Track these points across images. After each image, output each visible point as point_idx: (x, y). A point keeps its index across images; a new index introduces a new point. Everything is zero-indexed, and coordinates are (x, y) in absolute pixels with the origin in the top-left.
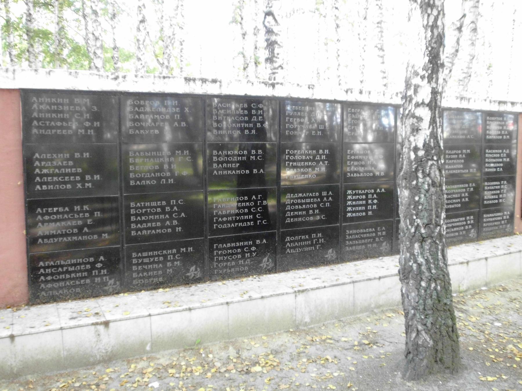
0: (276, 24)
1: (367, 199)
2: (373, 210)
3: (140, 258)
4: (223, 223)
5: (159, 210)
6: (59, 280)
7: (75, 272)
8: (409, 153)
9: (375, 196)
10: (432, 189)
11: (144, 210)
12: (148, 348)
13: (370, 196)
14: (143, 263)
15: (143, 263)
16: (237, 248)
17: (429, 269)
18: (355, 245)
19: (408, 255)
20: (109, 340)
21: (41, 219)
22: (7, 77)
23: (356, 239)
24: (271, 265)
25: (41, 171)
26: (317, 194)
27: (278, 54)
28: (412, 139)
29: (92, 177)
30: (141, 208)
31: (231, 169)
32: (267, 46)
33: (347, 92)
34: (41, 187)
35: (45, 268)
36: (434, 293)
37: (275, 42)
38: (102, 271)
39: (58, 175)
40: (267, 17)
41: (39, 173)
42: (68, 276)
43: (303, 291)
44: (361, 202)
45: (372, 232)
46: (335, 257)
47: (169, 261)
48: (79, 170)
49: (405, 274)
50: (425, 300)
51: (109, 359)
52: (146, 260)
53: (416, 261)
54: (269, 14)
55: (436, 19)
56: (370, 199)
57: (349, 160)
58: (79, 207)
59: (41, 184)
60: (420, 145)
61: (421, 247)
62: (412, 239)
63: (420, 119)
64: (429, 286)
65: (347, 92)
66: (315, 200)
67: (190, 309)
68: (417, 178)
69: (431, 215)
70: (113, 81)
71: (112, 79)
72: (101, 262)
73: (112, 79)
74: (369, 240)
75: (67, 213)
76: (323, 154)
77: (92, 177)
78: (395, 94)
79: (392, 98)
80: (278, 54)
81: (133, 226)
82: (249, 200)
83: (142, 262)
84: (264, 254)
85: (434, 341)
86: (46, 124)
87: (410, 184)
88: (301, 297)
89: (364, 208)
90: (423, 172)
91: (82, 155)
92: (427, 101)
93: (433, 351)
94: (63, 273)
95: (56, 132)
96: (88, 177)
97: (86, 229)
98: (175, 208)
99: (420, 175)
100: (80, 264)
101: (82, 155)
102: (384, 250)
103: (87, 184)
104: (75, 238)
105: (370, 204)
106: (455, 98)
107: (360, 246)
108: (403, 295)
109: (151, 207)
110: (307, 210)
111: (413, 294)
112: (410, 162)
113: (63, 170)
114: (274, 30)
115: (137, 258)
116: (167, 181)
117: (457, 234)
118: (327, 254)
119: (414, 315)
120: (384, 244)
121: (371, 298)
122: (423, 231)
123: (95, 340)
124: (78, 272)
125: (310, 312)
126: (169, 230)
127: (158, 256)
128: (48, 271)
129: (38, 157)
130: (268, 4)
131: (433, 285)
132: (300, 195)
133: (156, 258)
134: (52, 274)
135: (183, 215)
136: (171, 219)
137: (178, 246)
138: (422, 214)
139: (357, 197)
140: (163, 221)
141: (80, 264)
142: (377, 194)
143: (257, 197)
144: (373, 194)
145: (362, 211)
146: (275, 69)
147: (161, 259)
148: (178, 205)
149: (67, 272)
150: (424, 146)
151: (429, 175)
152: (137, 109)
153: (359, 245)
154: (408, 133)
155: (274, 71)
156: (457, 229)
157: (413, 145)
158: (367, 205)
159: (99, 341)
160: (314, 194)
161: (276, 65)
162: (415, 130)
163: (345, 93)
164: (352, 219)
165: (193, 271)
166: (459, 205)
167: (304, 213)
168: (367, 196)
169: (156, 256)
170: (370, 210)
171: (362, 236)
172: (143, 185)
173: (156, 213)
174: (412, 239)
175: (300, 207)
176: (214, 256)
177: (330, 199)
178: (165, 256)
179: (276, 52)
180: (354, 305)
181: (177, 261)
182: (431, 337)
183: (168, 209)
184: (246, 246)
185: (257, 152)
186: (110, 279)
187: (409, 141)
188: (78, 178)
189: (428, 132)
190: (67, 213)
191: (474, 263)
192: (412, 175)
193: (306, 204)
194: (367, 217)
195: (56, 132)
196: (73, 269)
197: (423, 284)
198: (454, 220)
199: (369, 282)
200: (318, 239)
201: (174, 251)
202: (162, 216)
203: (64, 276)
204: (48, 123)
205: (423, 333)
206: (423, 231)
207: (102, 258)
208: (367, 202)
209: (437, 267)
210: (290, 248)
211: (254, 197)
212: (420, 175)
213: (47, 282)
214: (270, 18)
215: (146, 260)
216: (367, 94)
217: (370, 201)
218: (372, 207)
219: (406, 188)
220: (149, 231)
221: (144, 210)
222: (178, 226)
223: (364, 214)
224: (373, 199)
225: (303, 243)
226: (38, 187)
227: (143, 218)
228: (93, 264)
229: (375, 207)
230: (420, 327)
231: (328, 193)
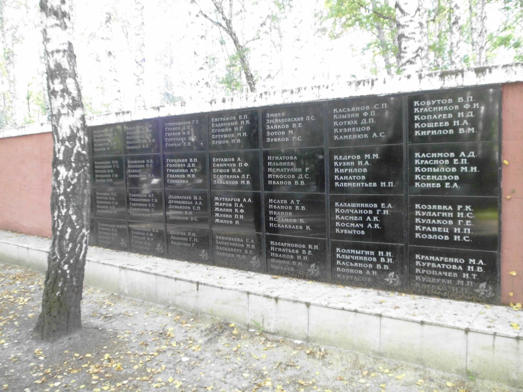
0: (403, 15)
1: (233, 208)
9: (241, 205)
13: (236, 205)
18: (225, 251)
23: (225, 246)
24: (398, 283)
26: (190, 198)
27: (405, 48)
33: (211, 103)
44: (227, 210)
56: (236, 208)
57: (215, 168)
65: (211, 103)
74: (238, 250)
76: (193, 162)
78: (259, 95)
79: (255, 101)
84: (482, 281)
88: (123, 271)
89: (231, 216)
102: (254, 264)
105: (237, 213)
106: (347, 84)
107: (230, 254)
117: (361, 272)
118: (200, 253)
120: (254, 258)
121: (169, 295)
125: (128, 286)
132: (178, 197)
139: (224, 204)
142: (244, 204)
143: (295, 202)
153: (229, 252)
156: (361, 265)
158: (233, 213)
160: (282, 201)
163: (210, 104)
166: (363, 232)
168: (233, 204)
170: (237, 219)
171: (353, 257)
172: (342, 187)
175: (178, 207)
177: (200, 203)
191: (286, 303)
193: (182, 205)
198: (353, 251)
199: (167, 279)
200: (193, 237)
208: (234, 210)
211: (292, 201)
216: (230, 101)
217: (236, 210)
218: (239, 217)
223: (447, 238)
224: (239, 209)
231: (198, 198)
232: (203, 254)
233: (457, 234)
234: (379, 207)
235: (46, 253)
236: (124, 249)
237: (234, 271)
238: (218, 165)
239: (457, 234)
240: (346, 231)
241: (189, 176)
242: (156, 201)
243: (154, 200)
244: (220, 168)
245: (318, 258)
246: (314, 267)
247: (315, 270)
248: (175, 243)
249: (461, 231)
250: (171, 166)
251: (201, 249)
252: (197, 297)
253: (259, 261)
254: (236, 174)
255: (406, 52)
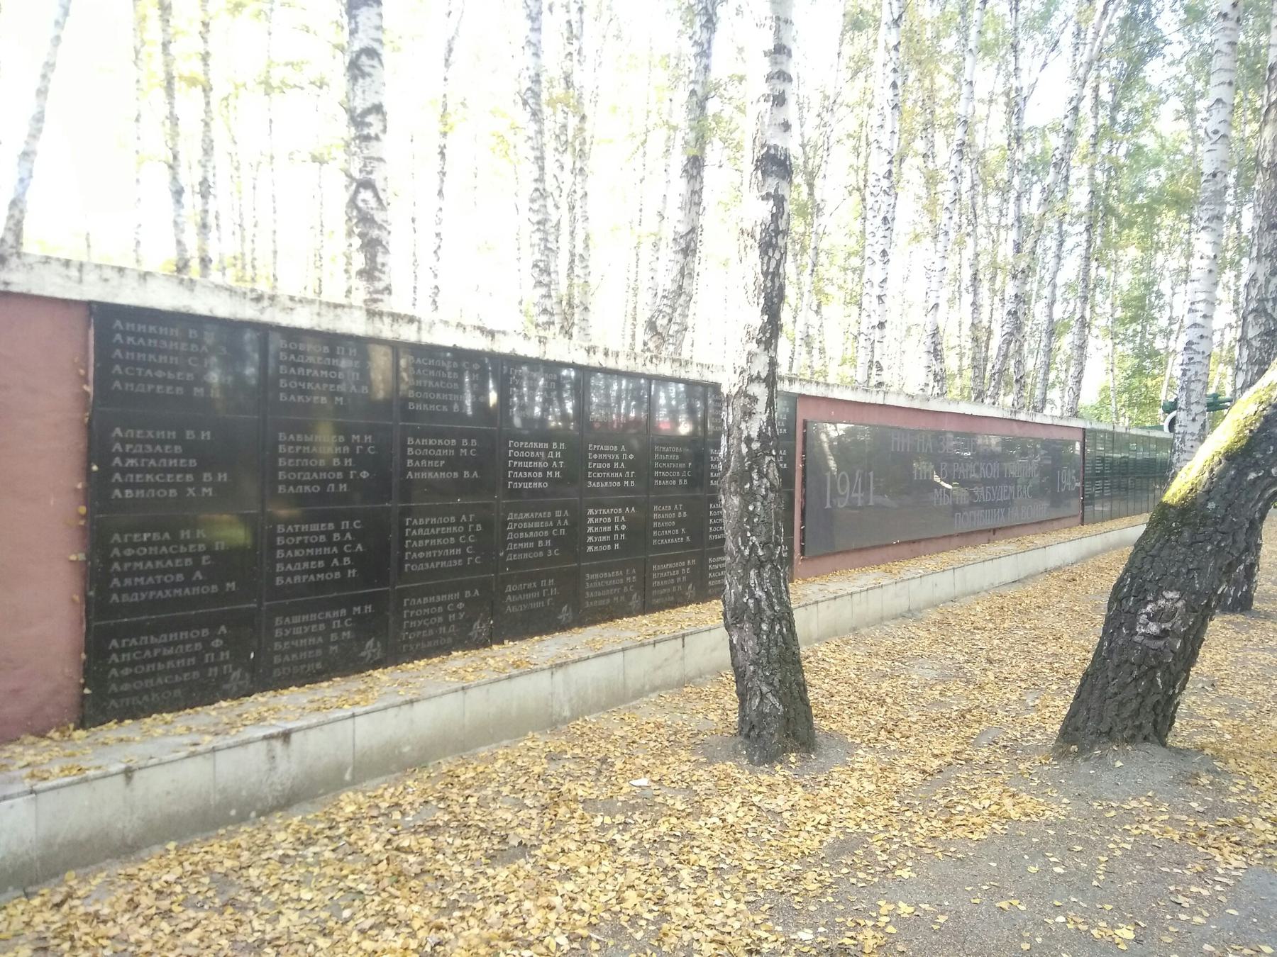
2: (620, 541)
3: (288, 626)
4: (418, 561)
5: (322, 538)
6: (144, 676)
7: (173, 657)
8: (739, 445)
10: (771, 495)
11: (299, 539)
12: (348, 777)
14: (292, 637)
15: (292, 637)
16: (437, 605)
17: (771, 606)
19: (740, 587)
20: (290, 765)
21: (118, 554)
22: (68, 277)
25: (124, 462)
26: (453, 519)
27: (383, 265)
28: (743, 426)
29: (215, 476)
30: (294, 535)
31: (434, 469)
32: (362, 247)
33: (588, 352)
34: (123, 494)
35: (119, 652)
36: (780, 639)
37: (378, 242)
38: (222, 654)
39: (154, 471)
40: (362, 190)
41: (121, 465)
42: (160, 666)
43: (561, 665)
45: (619, 577)
46: (571, 618)
47: (334, 631)
48: (193, 463)
49: (734, 618)
50: (768, 650)
51: (288, 800)
52: (297, 631)
53: (752, 596)
54: (367, 184)
55: (778, 265)
58: (188, 532)
59: (123, 487)
60: (754, 434)
61: (759, 575)
62: (747, 564)
63: (754, 399)
64: (772, 628)
66: (547, 525)
67: (411, 702)
68: (751, 479)
69: (770, 530)
70: (253, 304)
71: (252, 299)
72: (222, 636)
73: (252, 299)
75: (167, 544)
76: (558, 450)
77: (215, 476)
80: (383, 265)
81: (279, 567)
82: (458, 523)
83: (291, 634)
85: (784, 707)
86: (136, 372)
87: (742, 488)
88: (559, 675)
90: (760, 472)
91: (198, 434)
92: (763, 375)
93: (784, 721)
94: (150, 661)
95: (154, 390)
96: (207, 476)
97: (198, 575)
98: (348, 536)
99: (755, 476)
100: (184, 642)
101: (198, 434)
103: (204, 490)
104: (178, 592)
108: (732, 647)
109: (310, 533)
110: (535, 540)
111: (751, 643)
112: (741, 458)
113: (164, 460)
114: (376, 218)
115: (283, 627)
116: (337, 487)
119: (754, 672)
122: (760, 553)
123: (268, 766)
124: (180, 658)
125: (570, 700)
126: (338, 575)
127: (318, 622)
128: (126, 657)
129: (120, 434)
130: (365, 166)
131: (777, 628)
133: (314, 626)
134: (132, 664)
135: (359, 547)
136: (466, 533)
137: (349, 603)
138: (758, 529)
140: (328, 558)
141: (184, 642)
144: (620, 515)
145: (606, 543)
146: (377, 292)
147: (322, 627)
148: (353, 532)
149: (163, 659)
150: (759, 436)
151: (766, 476)
152: (292, 357)
154: (738, 418)
155: (375, 296)
157: (745, 434)
159: (273, 769)
161: (380, 285)
162: (748, 414)
164: (594, 555)
165: (371, 647)
167: (532, 545)
169: (313, 622)
173: (318, 545)
174: (747, 564)
176: (403, 620)
178: (328, 622)
179: (380, 259)
180: (625, 686)
181: (346, 629)
182: (781, 702)
183: (336, 536)
184: (451, 601)
185: (469, 442)
186: (235, 669)
187: (739, 428)
188: (189, 478)
189: (764, 418)
190: (167, 544)
192: (744, 476)
193: (533, 530)
194: (613, 553)
195: (154, 390)
196: (170, 652)
197: (764, 627)
200: (549, 588)
201: (343, 612)
202: (327, 550)
203: (153, 666)
204: (140, 370)
205: (769, 695)
206: (760, 553)
207: (223, 629)
209: (781, 603)
210: (512, 604)
212: (755, 476)
213: (121, 680)
214: (366, 195)
215: (297, 631)
219: (736, 493)
220: (305, 577)
221: (299, 539)
222: (351, 567)
224: (620, 524)
225: (528, 596)
226: (117, 492)
227: (297, 553)
228: (206, 642)
229: (623, 536)
230: (765, 689)
234: (338, 529)
238: (595, 456)
240: (443, 564)
241: (549, 473)
242: (479, 527)
243: (474, 528)
244: (598, 461)
248: (514, 609)
250: (517, 454)
252: (682, 658)
254: (618, 470)
255: (384, 273)
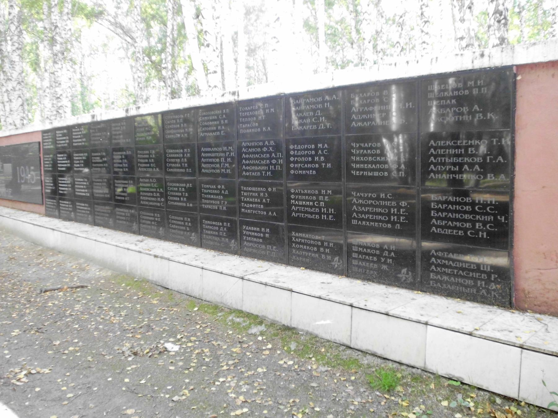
13: (262, 194)
24: (410, 280)
232: (233, 244)
233: (394, 215)
235: (523, 355)
236: (234, 253)
237: (213, 253)
239: (394, 215)
245: (232, 233)
246: (406, 272)
247: (407, 276)
249: (397, 211)
251: (404, 266)
253: (341, 262)
